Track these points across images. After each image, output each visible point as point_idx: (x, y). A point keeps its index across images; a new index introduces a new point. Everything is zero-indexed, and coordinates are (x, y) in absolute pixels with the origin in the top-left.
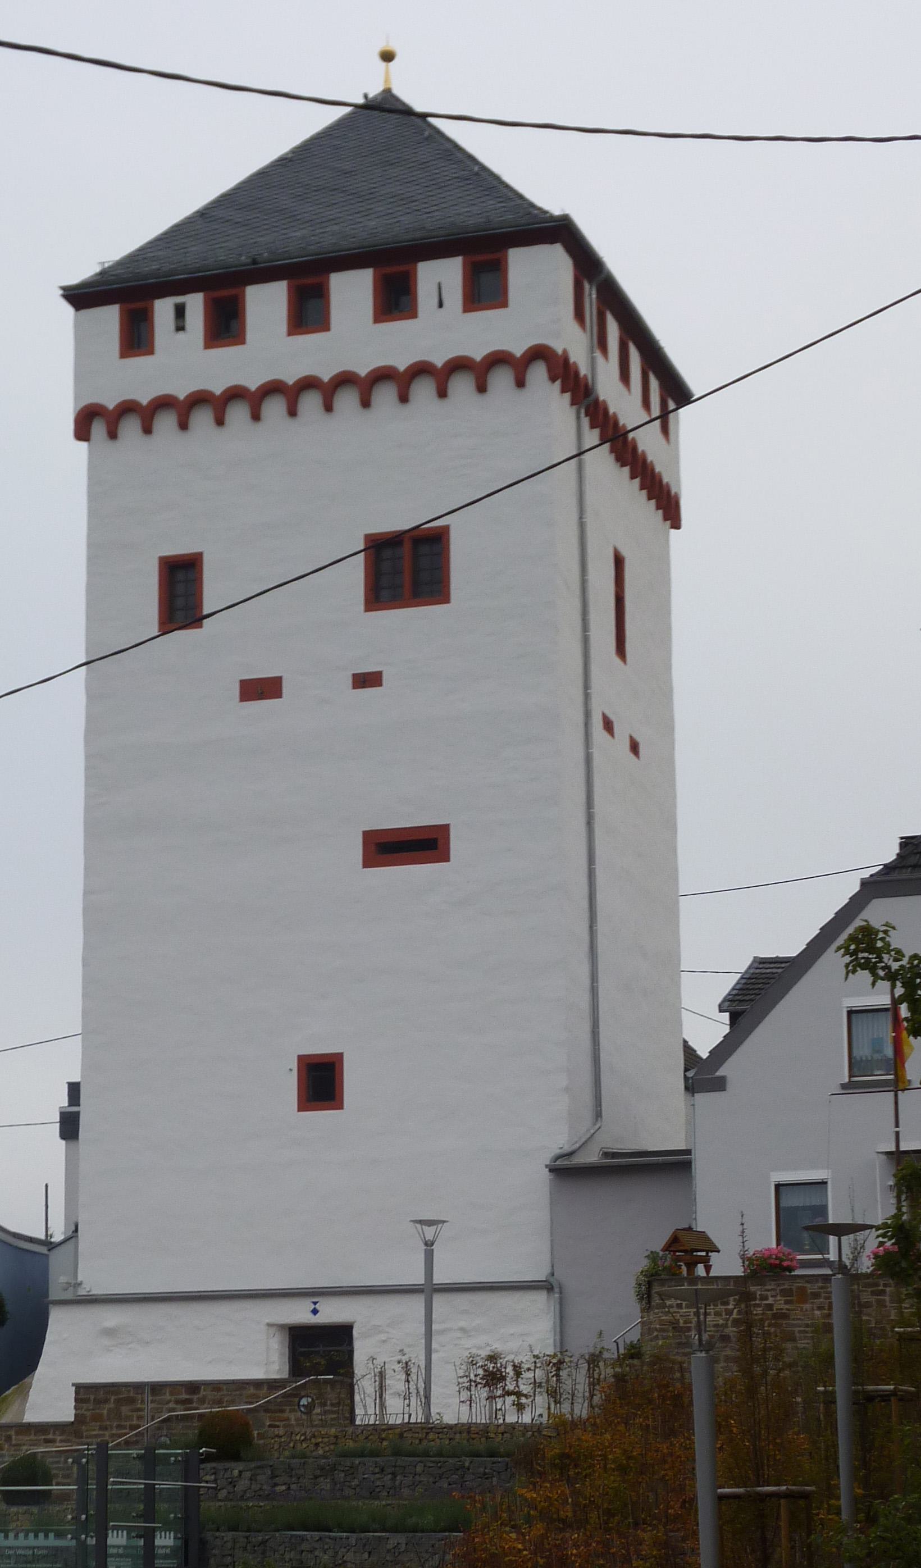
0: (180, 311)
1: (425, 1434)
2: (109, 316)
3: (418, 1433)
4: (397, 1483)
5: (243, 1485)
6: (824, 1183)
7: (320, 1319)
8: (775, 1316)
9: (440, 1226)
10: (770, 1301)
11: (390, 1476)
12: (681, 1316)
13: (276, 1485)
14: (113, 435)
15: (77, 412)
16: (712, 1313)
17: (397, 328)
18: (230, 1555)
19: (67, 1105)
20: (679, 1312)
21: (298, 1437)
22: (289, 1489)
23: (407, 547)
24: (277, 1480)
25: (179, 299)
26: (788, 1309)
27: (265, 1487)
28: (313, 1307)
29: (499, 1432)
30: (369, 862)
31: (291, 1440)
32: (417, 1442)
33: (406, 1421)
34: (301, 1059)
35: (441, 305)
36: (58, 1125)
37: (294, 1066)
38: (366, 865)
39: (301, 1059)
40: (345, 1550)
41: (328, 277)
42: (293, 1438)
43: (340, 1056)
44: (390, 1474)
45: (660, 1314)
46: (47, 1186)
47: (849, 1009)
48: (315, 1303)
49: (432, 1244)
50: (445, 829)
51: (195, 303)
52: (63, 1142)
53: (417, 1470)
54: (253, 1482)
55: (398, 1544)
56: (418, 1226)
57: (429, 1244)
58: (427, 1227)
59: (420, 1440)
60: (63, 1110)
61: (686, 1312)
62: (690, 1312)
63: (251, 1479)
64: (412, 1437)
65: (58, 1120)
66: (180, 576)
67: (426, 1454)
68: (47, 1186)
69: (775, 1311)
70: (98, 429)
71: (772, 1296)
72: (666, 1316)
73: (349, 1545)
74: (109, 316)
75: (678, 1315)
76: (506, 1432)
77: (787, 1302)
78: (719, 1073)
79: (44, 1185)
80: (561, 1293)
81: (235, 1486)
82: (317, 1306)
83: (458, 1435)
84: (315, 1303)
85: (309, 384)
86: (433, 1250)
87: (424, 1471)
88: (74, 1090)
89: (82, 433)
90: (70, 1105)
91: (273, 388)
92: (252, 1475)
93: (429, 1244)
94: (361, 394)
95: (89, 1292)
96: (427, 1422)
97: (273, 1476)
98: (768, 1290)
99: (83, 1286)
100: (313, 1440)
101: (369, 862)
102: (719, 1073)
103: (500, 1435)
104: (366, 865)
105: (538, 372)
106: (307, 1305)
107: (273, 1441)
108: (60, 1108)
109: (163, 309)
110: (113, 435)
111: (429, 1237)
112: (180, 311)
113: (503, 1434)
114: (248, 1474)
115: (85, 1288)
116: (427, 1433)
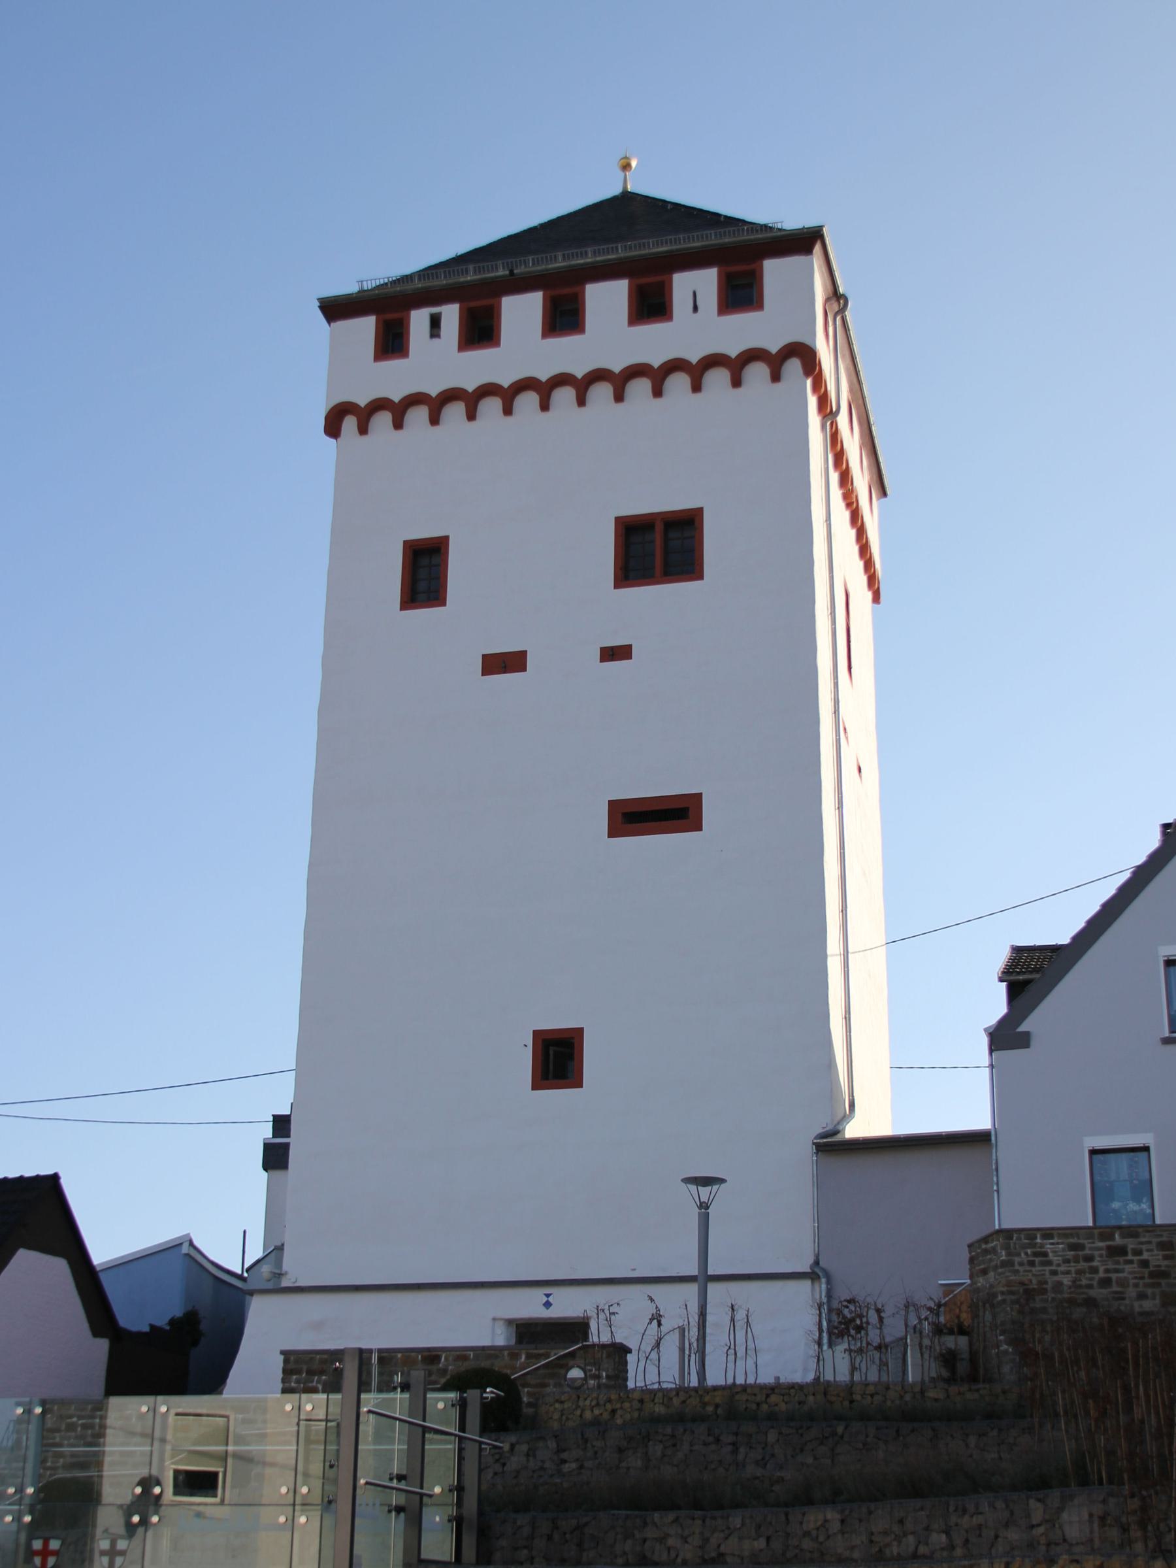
0: (435, 322)
1: (764, 1396)
2: (365, 327)
3: (755, 1395)
4: (741, 1457)
5: (514, 1462)
6: (1146, 1149)
7: (556, 1312)
8: (1152, 1275)
9: (715, 1187)
10: (1145, 1256)
11: (730, 1448)
12: (1034, 1275)
13: (564, 1461)
14: (363, 430)
15: (328, 410)
16: (1073, 1272)
17: (653, 330)
18: (525, 1547)
19: (271, 1136)
20: (1031, 1271)
21: (588, 1402)
22: (581, 1467)
23: (658, 535)
24: (565, 1455)
25: (435, 310)
26: (1167, 1266)
27: (547, 1465)
28: (545, 1299)
29: (867, 1392)
30: (614, 831)
31: (578, 1407)
32: (754, 1406)
33: (730, 1381)
34: (536, 1033)
35: (695, 309)
36: (272, 1123)
37: (530, 1041)
38: (611, 834)
39: (536, 1033)
40: (722, 1535)
41: (584, 289)
42: (581, 1403)
43: (580, 1031)
44: (730, 1444)
45: (1009, 1274)
46: (245, 1232)
47: (1166, 958)
48: (548, 1295)
49: (707, 1207)
50: (698, 797)
51: (451, 314)
52: (265, 1174)
53: (769, 1439)
54: (531, 1459)
55: (826, 1521)
56: (693, 1188)
57: (704, 1206)
58: (701, 1188)
59: (758, 1404)
60: (267, 1141)
61: (1040, 1271)
62: (1045, 1270)
63: (528, 1455)
64: (747, 1400)
65: (272, 1120)
66: (424, 561)
67: (772, 1417)
68: (245, 1232)
69: (1152, 1269)
70: (350, 424)
71: (1148, 1250)
72: (1015, 1276)
73: (729, 1528)
74: (365, 327)
75: (1030, 1274)
76: (877, 1393)
77: (1166, 1257)
78: (1023, 1028)
79: (243, 1231)
80: (828, 1282)
81: (504, 1465)
82: (551, 1299)
83: (811, 1398)
84: (548, 1295)
85: (562, 380)
86: (708, 1213)
87: (778, 1440)
88: (281, 1124)
89: (333, 427)
90: (274, 1136)
91: (526, 385)
92: (529, 1449)
93: (704, 1206)
94: (615, 390)
95: (294, 1283)
96: (1142, 1202)
97: (560, 1450)
98: (1142, 1243)
99: (288, 1277)
100: (609, 1406)
101: (614, 831)
102: (1023, 1028)
103: (869, 1397)
104: (611, 834)
105: (794, 366)
106: (538, 1294)
107: (552, 1409)
108: (264, 1139)
109: (419, 319)
110: (363, 430)
111: (704, 1199)
112: (435, 322)
113: (872, 1396)
114: (524, 1448)
115: (290, 1279)
116: (768, 1396)
